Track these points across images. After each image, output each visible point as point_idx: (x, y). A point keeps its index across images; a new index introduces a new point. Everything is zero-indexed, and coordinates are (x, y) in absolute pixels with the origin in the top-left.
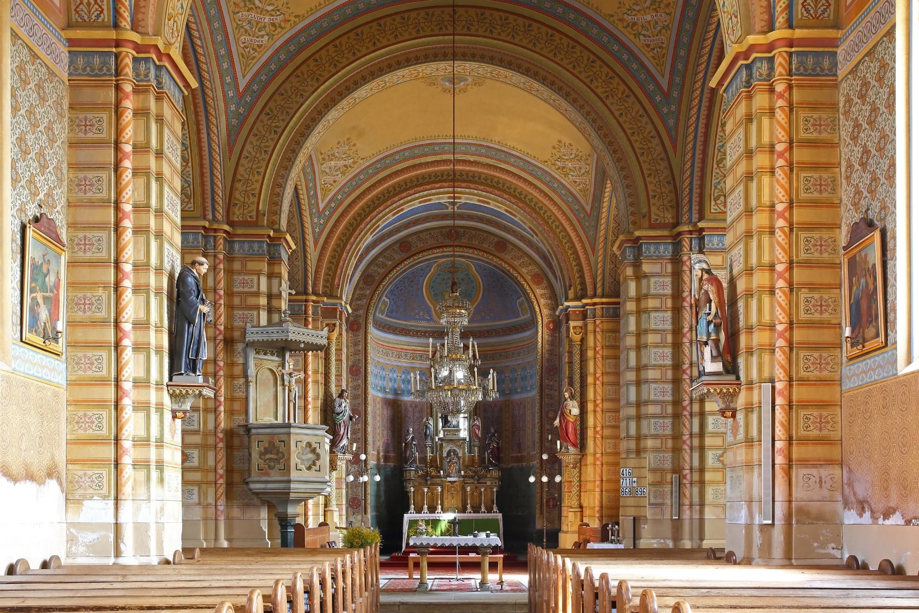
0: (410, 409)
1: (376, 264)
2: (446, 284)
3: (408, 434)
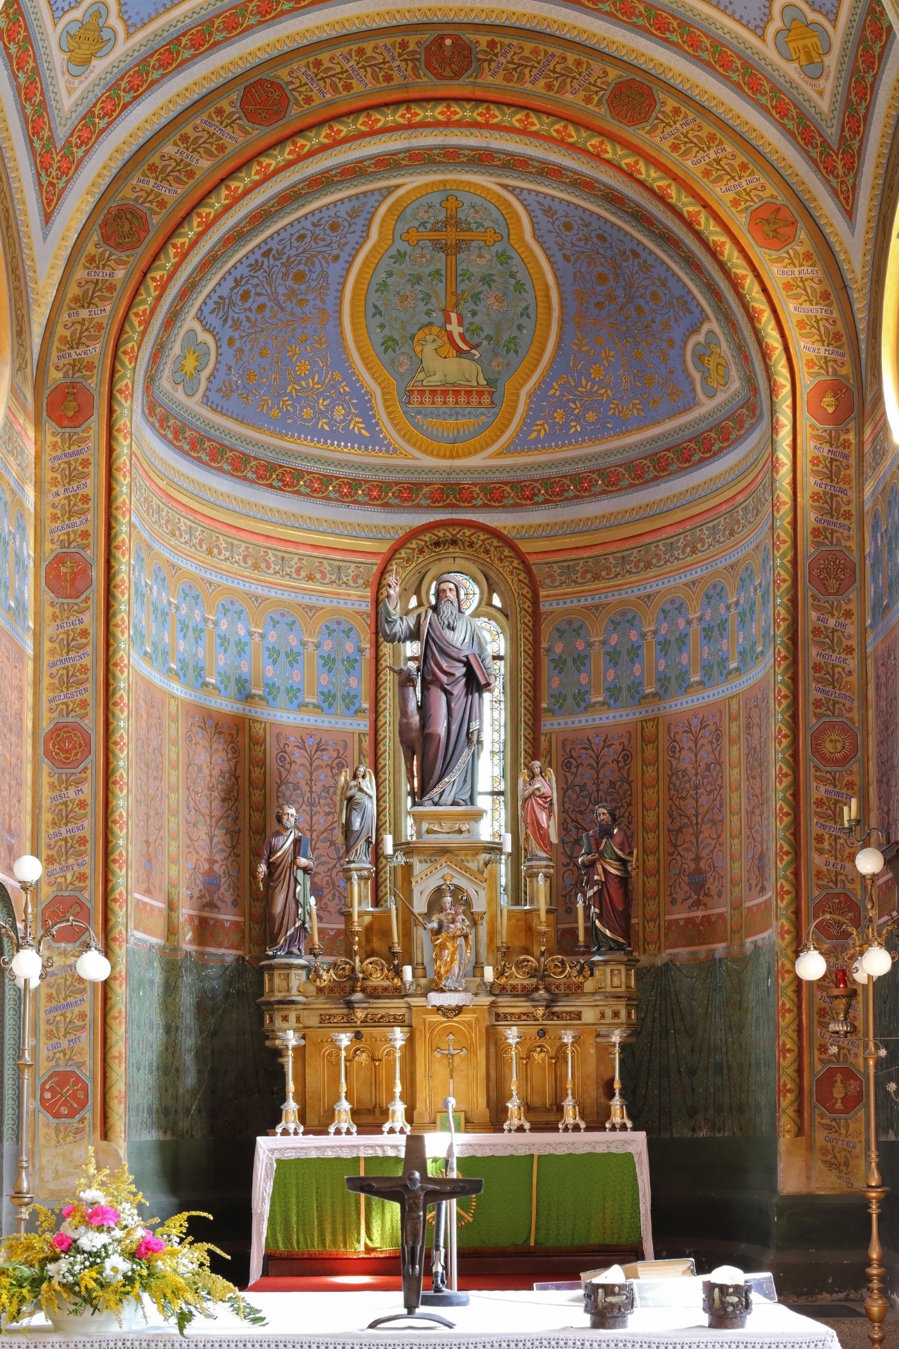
0: (298, 756)
1: (153, 168)
2: (426, 299)
3: (282, 829)
